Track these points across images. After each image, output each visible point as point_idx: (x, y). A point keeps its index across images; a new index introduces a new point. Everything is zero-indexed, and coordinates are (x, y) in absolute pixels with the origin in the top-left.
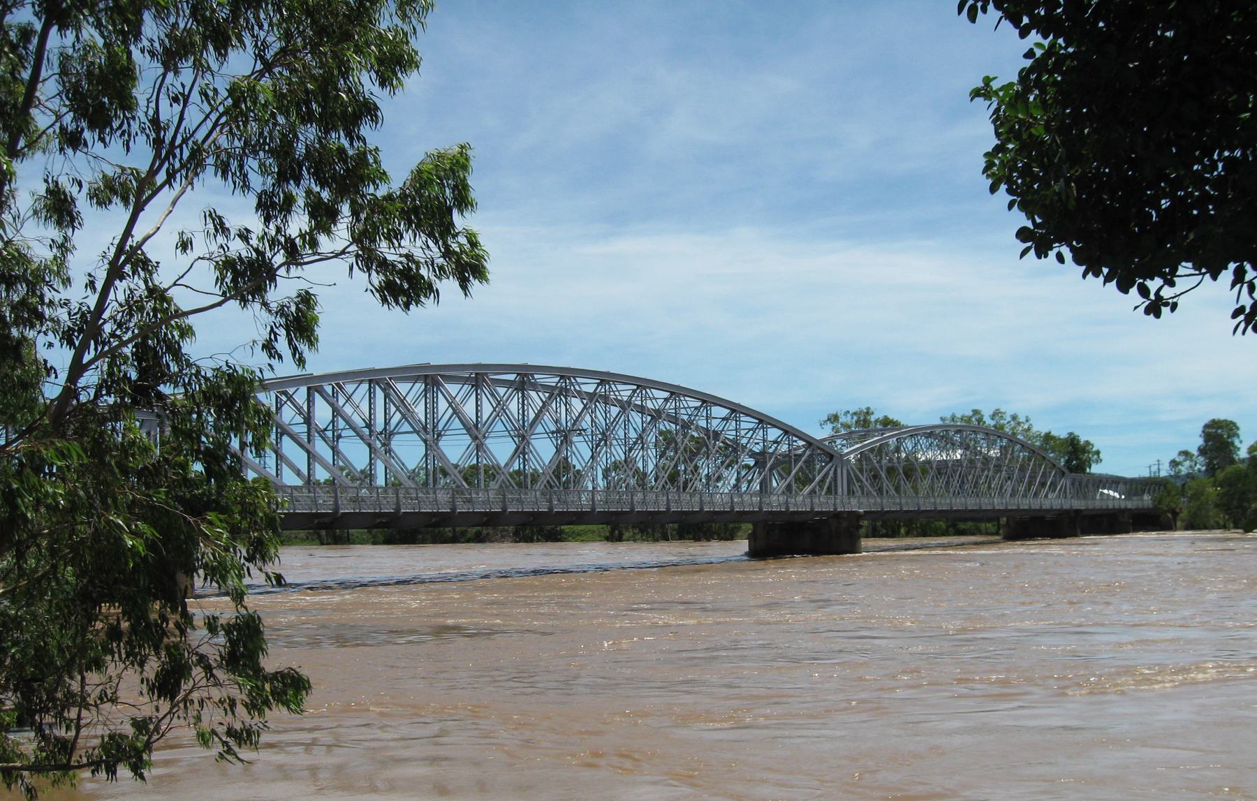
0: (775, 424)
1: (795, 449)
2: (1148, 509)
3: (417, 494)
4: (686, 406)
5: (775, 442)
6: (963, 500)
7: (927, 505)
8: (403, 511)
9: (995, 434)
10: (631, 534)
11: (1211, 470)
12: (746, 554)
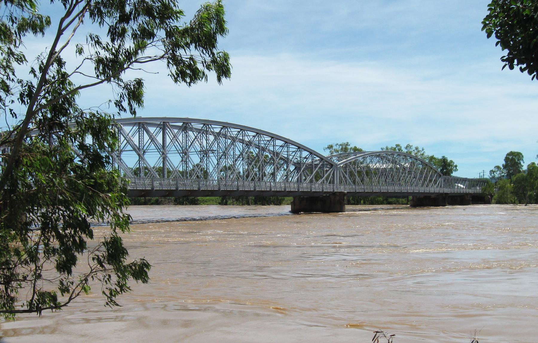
0: (306, 149)
1: (315, 162)
2: (479, 193)
3: (135, 181)
4: (264, 140)
5: (305, 158)
6: (386, 187)
7: (376, 189)
8: (155, 189)
9: (407, 156)
10: (231, 201)
11: (509, 175)
12: (290, 212)
